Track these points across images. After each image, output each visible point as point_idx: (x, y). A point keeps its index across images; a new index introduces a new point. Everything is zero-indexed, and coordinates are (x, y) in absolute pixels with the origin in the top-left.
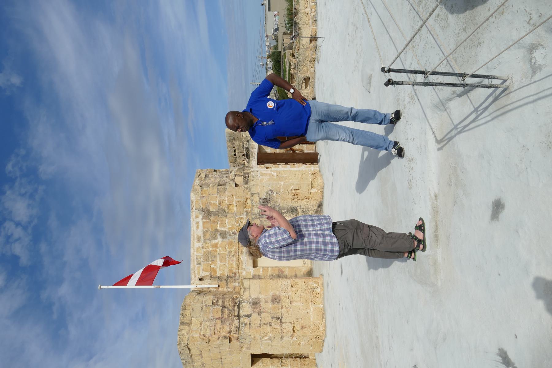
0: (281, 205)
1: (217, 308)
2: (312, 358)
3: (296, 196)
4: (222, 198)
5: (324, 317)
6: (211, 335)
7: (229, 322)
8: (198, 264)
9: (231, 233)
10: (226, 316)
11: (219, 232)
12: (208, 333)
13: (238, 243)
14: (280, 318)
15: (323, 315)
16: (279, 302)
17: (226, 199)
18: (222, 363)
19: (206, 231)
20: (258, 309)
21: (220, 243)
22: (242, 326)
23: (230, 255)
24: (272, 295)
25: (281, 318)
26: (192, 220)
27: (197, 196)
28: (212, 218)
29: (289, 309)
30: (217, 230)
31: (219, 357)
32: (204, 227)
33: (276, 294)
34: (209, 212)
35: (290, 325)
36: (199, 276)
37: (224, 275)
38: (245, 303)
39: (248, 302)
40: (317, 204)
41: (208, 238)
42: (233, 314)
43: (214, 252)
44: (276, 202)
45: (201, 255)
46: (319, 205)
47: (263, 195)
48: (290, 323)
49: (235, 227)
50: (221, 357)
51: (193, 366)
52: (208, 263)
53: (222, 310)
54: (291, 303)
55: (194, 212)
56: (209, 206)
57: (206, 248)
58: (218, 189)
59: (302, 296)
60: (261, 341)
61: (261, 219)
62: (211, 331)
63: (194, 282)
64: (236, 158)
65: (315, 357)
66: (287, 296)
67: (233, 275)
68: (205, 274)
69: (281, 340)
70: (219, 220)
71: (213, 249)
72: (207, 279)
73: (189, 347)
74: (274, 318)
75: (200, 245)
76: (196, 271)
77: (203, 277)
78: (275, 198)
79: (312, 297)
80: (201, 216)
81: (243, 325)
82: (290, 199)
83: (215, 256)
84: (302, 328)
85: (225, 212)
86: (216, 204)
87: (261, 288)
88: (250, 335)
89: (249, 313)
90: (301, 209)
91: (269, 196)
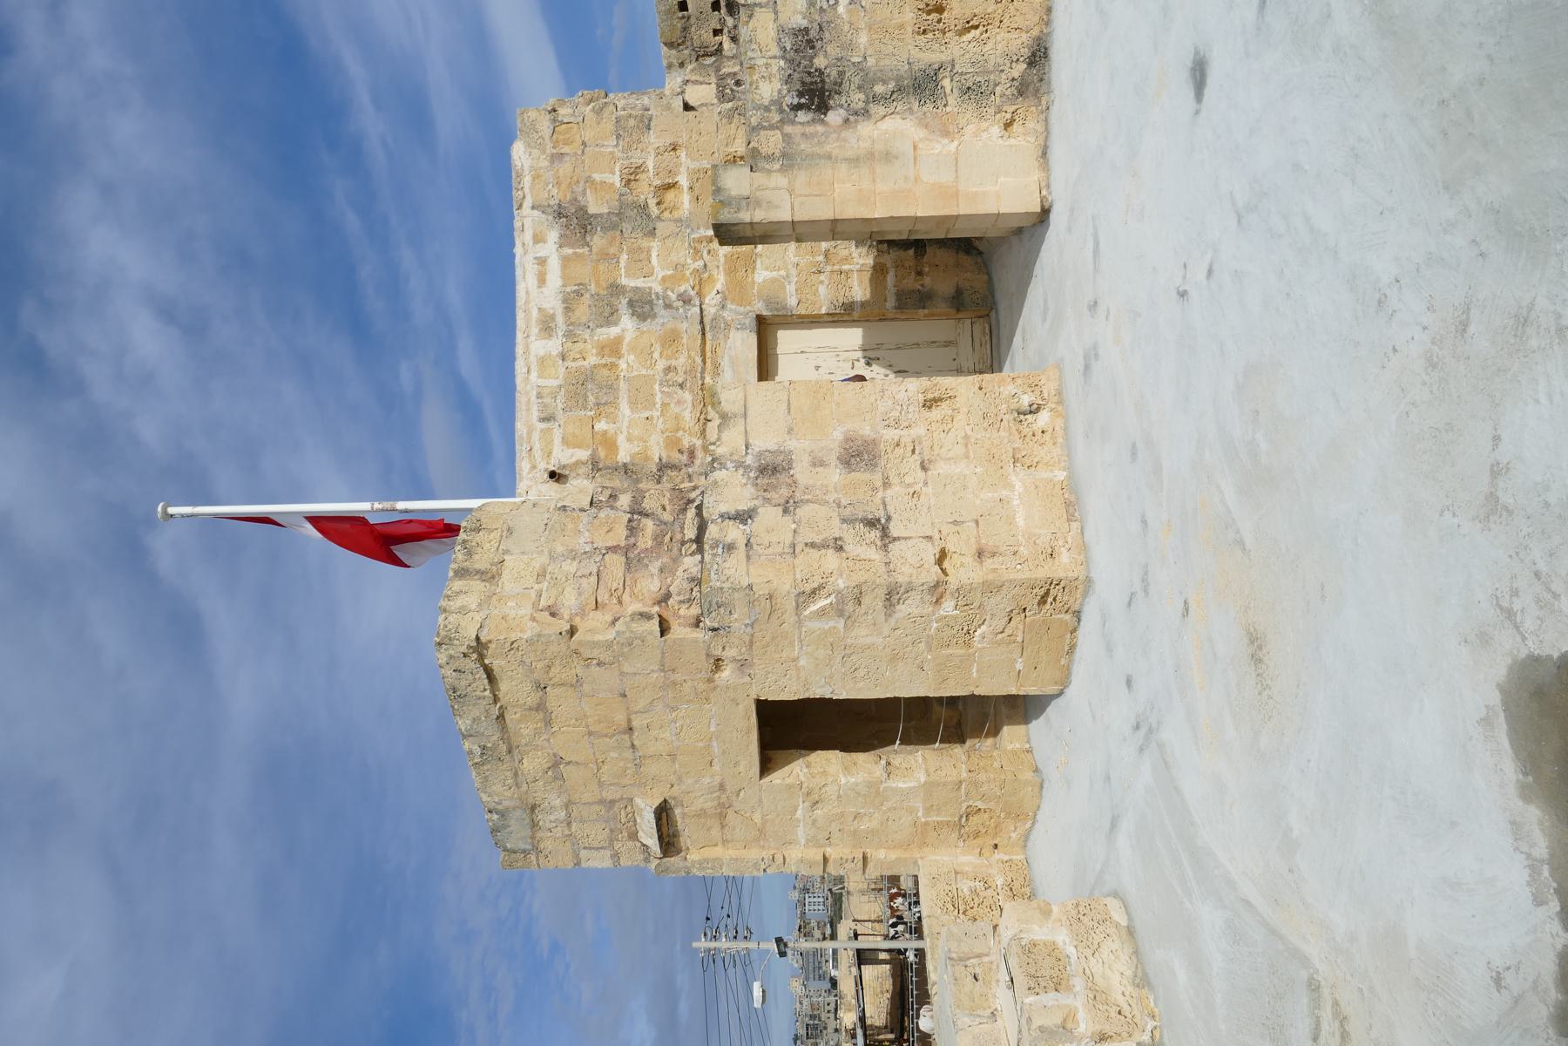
0: (871, 61)
1: (607, 517)
2: (1018, 746)
3: (935, 16)
4: (633, 160)
5: (1076, 514)
6: (582, 613)
7: (658, 564)
8: (543, 420)
9: (673, 296)
10: (645, 541)
11: (624, 294)
12: (570, 601)
13: (700, 337)
14: (879, 520)
15: (1072, 508)
16: (872, 464)
17: (650, 164)
18: (637, 754)
19: (575, 291)
20: (784, 492)
21: (628, 337)
22: (715, 555)
23: (667, 381)
24: (841, 437)
25: (883, 521)
26: (518, 250)
27: (536, 152)
28: (598, 240)
29: (917, 488)
30: (616, 289)
31: (620, 718)
32: (566, 278)
33: (861, 432)
34: (586, 217)
35: (925, 544)
36: (548, 463)
37: (647, 459)
38: (724, 471)
39: (740, 465)
40: (1026, 52)
41: (584, 319)
42: (678, 536)
43: (605, 372)
44: (850, 47)
45: (555, 383)
46: (1034, 55)
47: (795, 12)
48: (924, 538)
49: (688, 273)
50: (629, 721)
51: (516, 774)
52: (583, 413)
53: (630, 521)
54: (924, 468)
55: (528, 221)
56: (584, 194)
57: (574, 360)
58: (618, 120)
59: (973, 440)
60: (799, 623)
61: (788, 129)
62: (580, 595)
63: (530, 487)
64: (689, 18)
65: (1028, 742)
66: (906, 440)
67: (684, 458)
68: (572, 456)
69: (888, 616)
70: (625, 248)
71: (603, 361)
72: (578, 475)
73: (486, 661)
74: (856, 520)
75: (554, 345)
76: (537, 446)
77: (564, 467)
78: (846, 28)
79: (1018, 444)
80: (553, 236)
81: (720, 550)
82: (910, 30)
83: (611, 388)
84: (980, 554)
85: (649, 216)
86: (613, 184)
87: (792, 412)
88: (750, 587)
89: (743, 507)
90: (956, 78)
91: (817, 17)
